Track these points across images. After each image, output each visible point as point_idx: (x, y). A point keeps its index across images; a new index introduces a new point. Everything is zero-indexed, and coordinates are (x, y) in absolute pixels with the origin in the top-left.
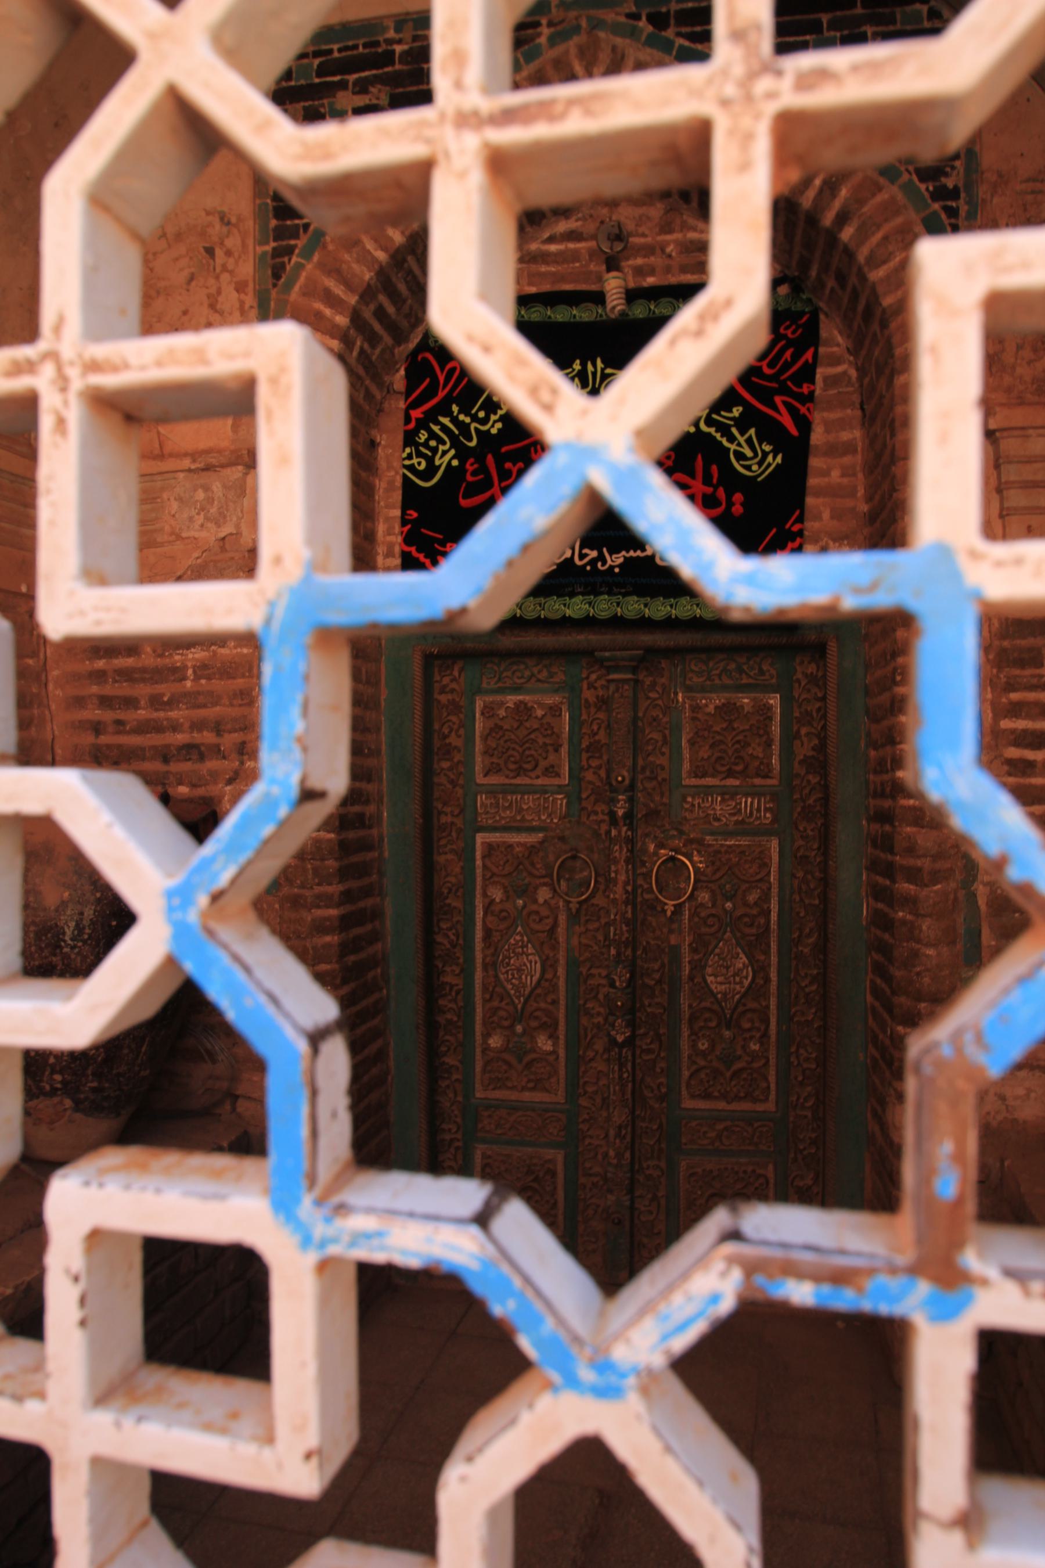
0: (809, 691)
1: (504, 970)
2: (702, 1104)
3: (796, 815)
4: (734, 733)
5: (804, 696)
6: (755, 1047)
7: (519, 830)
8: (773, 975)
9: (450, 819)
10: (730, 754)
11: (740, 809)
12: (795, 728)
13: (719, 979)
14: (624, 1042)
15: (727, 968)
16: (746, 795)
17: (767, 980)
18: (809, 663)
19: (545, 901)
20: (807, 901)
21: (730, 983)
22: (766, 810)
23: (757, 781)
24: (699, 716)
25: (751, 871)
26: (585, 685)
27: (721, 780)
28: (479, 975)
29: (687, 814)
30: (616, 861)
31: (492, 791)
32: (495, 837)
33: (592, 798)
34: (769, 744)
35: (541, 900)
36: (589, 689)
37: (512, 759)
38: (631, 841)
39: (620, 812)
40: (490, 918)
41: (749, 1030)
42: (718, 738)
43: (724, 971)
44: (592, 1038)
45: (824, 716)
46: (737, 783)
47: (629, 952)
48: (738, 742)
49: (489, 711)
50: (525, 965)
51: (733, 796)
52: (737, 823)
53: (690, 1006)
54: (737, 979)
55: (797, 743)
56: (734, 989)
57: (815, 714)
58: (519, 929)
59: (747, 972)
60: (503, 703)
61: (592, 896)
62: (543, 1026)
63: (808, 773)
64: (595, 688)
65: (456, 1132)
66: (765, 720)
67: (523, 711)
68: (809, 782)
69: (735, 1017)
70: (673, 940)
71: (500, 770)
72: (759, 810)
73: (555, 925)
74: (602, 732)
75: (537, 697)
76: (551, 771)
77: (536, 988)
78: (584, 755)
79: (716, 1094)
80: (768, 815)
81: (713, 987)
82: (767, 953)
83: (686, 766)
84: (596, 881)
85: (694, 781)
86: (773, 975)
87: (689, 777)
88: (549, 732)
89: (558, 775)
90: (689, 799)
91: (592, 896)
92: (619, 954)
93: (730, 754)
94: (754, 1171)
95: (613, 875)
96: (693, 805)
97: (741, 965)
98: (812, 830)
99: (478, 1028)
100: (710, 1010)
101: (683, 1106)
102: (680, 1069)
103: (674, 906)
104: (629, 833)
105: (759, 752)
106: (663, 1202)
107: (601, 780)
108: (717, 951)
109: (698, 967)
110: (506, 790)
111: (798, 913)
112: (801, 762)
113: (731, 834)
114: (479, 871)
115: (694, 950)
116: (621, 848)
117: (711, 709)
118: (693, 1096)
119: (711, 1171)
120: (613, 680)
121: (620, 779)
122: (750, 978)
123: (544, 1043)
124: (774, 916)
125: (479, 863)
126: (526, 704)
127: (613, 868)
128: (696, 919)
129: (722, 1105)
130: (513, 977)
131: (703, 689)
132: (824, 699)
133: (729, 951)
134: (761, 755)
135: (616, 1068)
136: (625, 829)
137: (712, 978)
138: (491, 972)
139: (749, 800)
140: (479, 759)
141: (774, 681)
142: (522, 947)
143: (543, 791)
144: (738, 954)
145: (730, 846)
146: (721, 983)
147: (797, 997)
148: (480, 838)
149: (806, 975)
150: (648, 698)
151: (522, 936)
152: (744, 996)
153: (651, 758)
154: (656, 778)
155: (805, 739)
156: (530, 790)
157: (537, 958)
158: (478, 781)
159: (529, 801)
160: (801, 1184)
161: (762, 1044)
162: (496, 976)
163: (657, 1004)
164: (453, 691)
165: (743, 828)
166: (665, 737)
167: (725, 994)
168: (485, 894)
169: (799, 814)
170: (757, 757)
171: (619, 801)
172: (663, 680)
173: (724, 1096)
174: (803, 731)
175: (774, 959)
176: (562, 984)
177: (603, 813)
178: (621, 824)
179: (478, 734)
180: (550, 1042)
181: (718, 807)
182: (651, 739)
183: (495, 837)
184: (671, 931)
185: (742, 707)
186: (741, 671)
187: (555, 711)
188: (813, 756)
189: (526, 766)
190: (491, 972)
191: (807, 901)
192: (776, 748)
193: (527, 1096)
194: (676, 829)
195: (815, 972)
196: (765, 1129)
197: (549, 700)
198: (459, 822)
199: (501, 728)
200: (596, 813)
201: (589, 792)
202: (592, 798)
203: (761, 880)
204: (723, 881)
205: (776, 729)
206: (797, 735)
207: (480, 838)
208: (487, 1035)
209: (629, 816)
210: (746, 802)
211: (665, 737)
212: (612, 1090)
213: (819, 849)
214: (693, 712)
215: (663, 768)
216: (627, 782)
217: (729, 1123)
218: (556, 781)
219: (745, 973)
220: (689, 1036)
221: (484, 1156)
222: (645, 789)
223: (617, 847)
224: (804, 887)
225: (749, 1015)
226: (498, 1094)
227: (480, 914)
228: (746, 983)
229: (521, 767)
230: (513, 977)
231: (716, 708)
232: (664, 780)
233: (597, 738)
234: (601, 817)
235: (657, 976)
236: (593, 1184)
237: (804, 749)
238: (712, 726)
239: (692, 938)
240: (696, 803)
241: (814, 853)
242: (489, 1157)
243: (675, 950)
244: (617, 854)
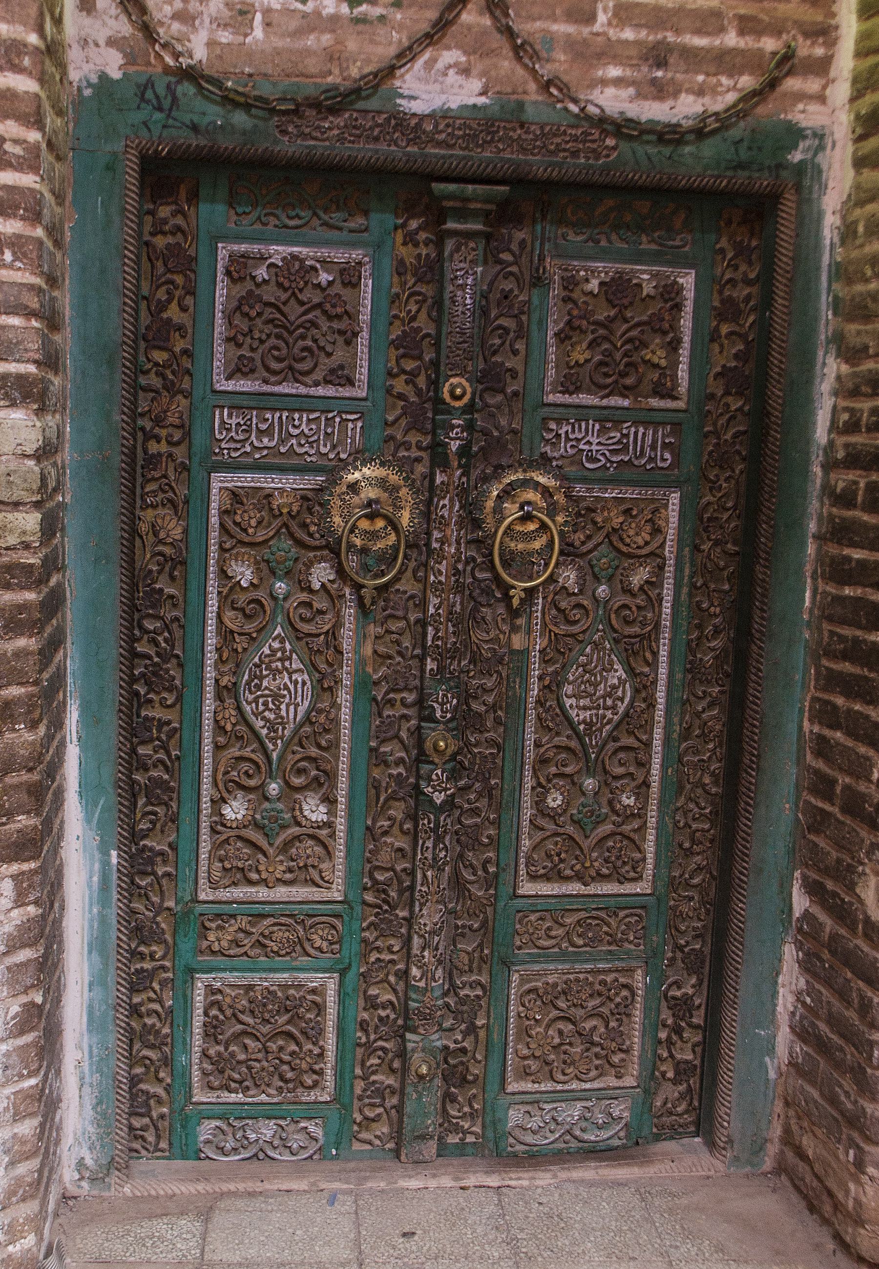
1: (251, 698)
2: (545, 889)
4: (625, 326)
6: (628, 800)
7: (282, 469)
8: (661, 696)
9: (163, 448)
10: (618, 358)
13: (582, 702)
14: (444, 802)
15: (596, 685)
16: (636, 423)
19: (323, 585)
20: (713, 586)
22: (665, 445)
23: (655, 402)
24: (574, 295)
26: (399, 238)
27: (602, 398)
28: (209, 705)
29: (548, 449)
30: (443, 523)
31: (239, 403)
32: (245, 480)
33: (403, 422)
34: (674, 346)
35: (316, 586)
36: (405, 244)
37: (276, 353)
38: (463, 492)
39: (454, 446)
40: (229, 614)
42: (602, 332)
43: (591, 690)
44: (387, 800)
46: (626, 403)
48: (630, 340)
49: (239, 268)
50: (286, 687)
51: (618, 424)
53: (538, 745)
54: (609, 702)
56: (604, 717)
58: (279, 630)
59: (624, 692)
60: (263, 258)
61: (396, 579)
62: (315, 784)
63: (727, 393)
64: (416, 245)
65: (163, 958)
66: (672, 308)
67: (295, 273)
70: (518, 642)
71: (252, 371)
72: (653, 447)
73: (338, 624)
74: (423, 315)
75: (323, 252)
76: (341, 376)
77: (302, 725)
78: (393, 354)
79: (568, 872)
80: (667, 455)
81: (573, 713)
82: (654, 665)
84: (405, 556)
85: (560, 398)
86: (661, 696)
87: (554, 391)
88: (339, 310)
89: (350, 382)
90: (553, 426)
91: (396, 579)
92: (441, 669)
93: (618, 358)
94: (616, 980)
95: (435, 545)
96: (558, 436)
97: (616, 681)
99: (207, 789)
100: (568, 749)
101: (520, 892)
102: (518, 838)
103: (525, 590)
104: (464, 479)
105: (659, 357)
106: (482, 1034)
107: (419, 392)
109: (552, 686)
110: (262, 402)
112: (717, 375)
113: (613, 481)
114: (214, 536)
115: (545, 661)
116: (451, 500)
117: (594, 285)
118: (533, 877)
119: (556, 985)
122: (627, 700)
123: (314, 810)
125: (214, 520)
126: (302, 261)
127: (436, 534)
129: (575, 888)
130: (267, 709)
133: (599, 659)
134: (663, 363)
135: (429, 844)
136: (459, 472)
137: (573, 701)
138: (229, 701)
140: (219, 349)
142: (281, 660)
143: (325, 405)
144: (611, 663)
146: (585, 708)
148: (219, 482)
151: (282, 642)
152: (616, 727)
153: (498, 359)
156: (302, 404)
157: (306, 677)
158: (218, 387)
159: (303, 423)
160: (678, 994)
161: (637, 795)
162: (239, 708)
164: (179, 229)
165: (624, 473)
166: (520, 325)
167: (589, 724)
168: (223, 573)
170: (656, 366)
171: (453, 427)
173: (579, 877)
174: (725, 329)
175: (663, 671)
176: (345, 715)
177: (419, 448)
179: (219, 307)
180: (323, 809)
181: (594, 441)
182: (500, 327)
183: (245, 480)
184: (515, 629)
185: (639, 286)
187: (349, 277)
189: (298, 366)
190: (229, 701)
191: (713, 586)
192: (684, 353)
193: (281, 893)
196: (633, 920)
197: (362, 374)
198: (179, 453)
199: (259, 299)
200: (407, 446)
201: (399, 412)
202: (403, 422)
203: (652, 554)
205: (686, 323)
206: (714, 336)
207: (219, 482)
208: (218, 802)
209: (465, 451)
210: (636, 433)
211: (520, 325)
212: (419, 876)
213: (735, 508)
214: (565, 288)
217: (583, 914)
218: (346, 392)
219: (620, 693)
220: (533, 788)
221: (211, 990)
222: (487, 406)
226: (240, 892)
227: (213, 603)
228: (622, 708)
229: (291, 368)
230: (267, 709)
231: (601, 284)
232: (516, 394)
233: (415, 325)
234: (415, 453)
235: (490, 699)
236: (381, 1019)
237: (724, 357)
238: (593, 313)
239: (546, 642)
240: (562, 432)
241: (725, 516)
242: (220, 991)
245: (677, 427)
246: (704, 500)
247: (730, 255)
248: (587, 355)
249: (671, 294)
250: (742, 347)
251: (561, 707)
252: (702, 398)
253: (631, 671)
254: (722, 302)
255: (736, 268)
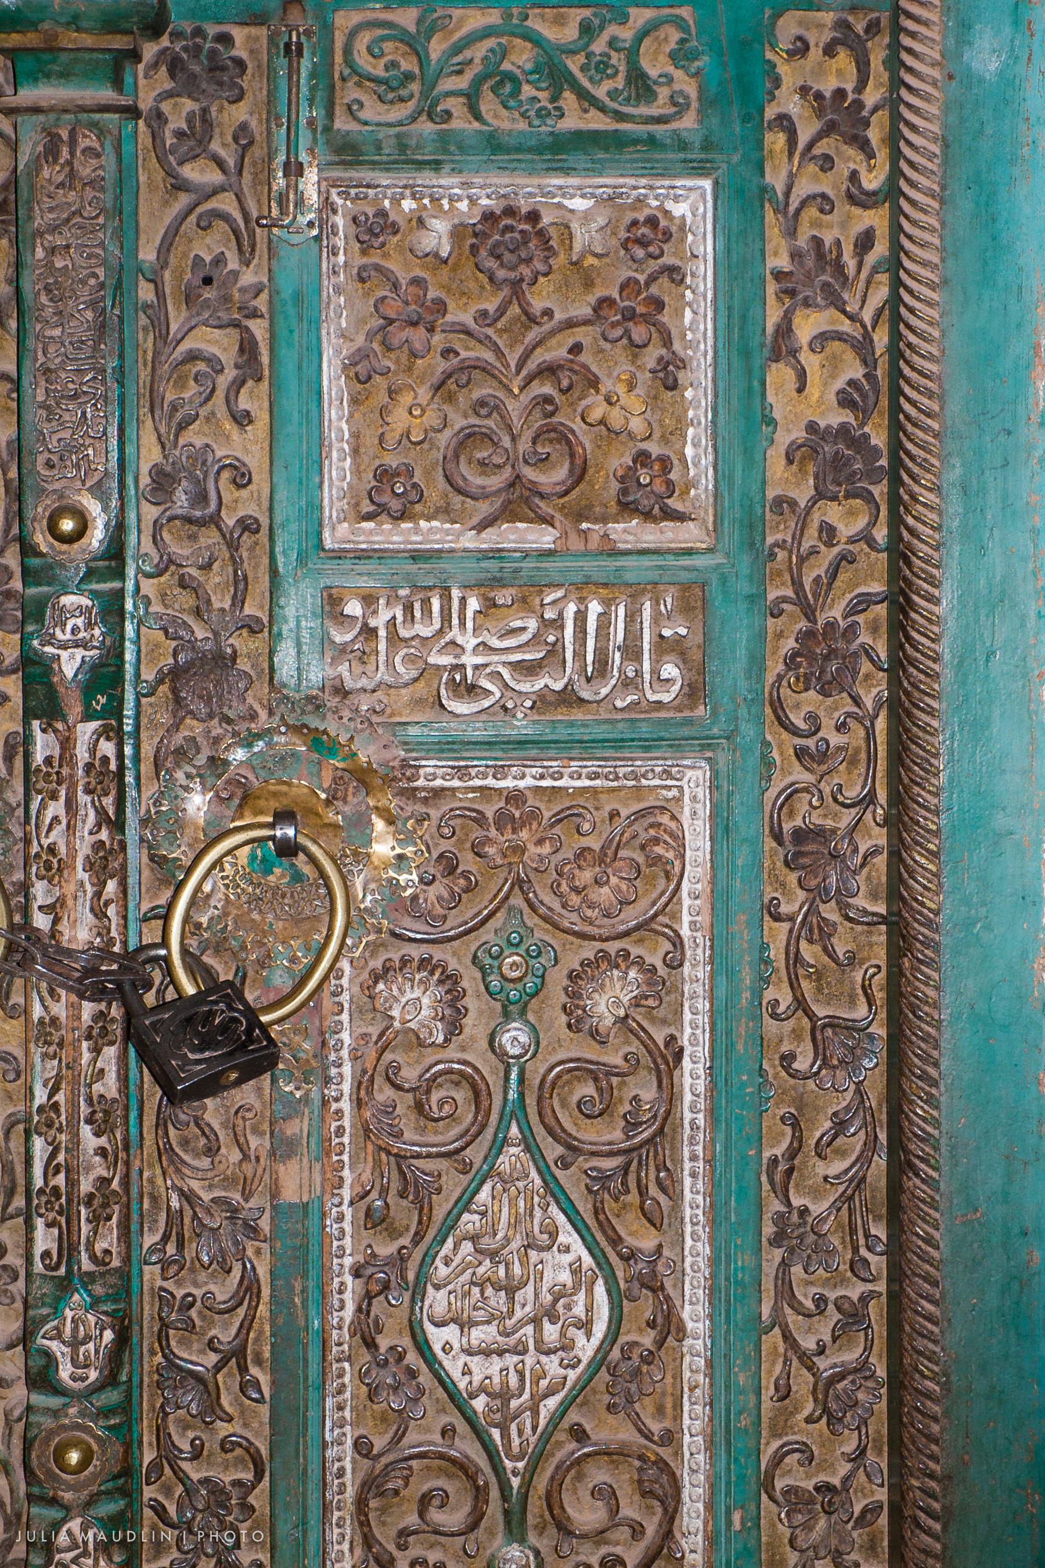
0: (827, 163)
3: (775, 667)
5: (803, 188)
8: (695, 1315)
11: (555, 651)
12: (773, 316)
13: (479, 1335)
15: (511, 1290)
16: (582, 588)
17: (668, 1326)
18: (829, 51)
21: (520, 1350)
23: (627, 532)
25: (604, 895)
30: (54, 867)
39: (70, 664)
41: (599, 1536)
43: (498, 1300)
45: (894, 264)
47: (108, 1240)
48: (550, 371)
52: (543, 701)
53: (362, 1447)
55: (780, 375)
57: (850, 263)
63: (820, 495)
68: (828, 533)
69: (541, 1483)
70: (294, 1181)
72: (631, 651)
80: (670, 670)
81: (453, 1367)
83: (339, 472)
86: (695, 1315)
90: (354, 608)
92: (68, 1247)
96: (370, 632)
98: (841, 728)
108: (470, 1221)
111: (787, 1060)
116: (71, 805)
117: (438, 236)
120: (36, 110)
121: (67, 525)
122: (600, 1329)
124: (693, 1076)
128: (384, 1094)
131: (406, 157)
132: (891, 193)
134: (637, 425)
136: (86, 730)
137: (450, 1333)
139: (595, 608)
141: (688, 122)
144: (553, 1234)
145: (515, 797)
146: (487, 1353)
147: (784, 1393)
149: (821, 1301)
150: (180, 186)
153: (194, 437)
154: (214, 520)
155: (810, 361)
163: (226, 1446)
166: (248, 348)
167: (504, 1395)
169: (791, 661)
172: (240, 113)
174: (807, 326)
175: (696, 1250)
178: (75, 709)
184: (283, 1149)
186: (557, 78)
188: (844, 428)
194: (298, 729)
195: (855, 1291)
204: (487, 934)
205: (696, 322)
206: (782, 345)
210: (581, 617)
211: (248, 348)
215: (242, 478)
216: (97, 537)
223: (56, 808)
224: (809, 952)
225: (599, 1475)
228: (586, 1348)
231: (458, 233)
235: (226, 1333)
240: (379, 621)
241: (848, 817)
243: (300, 1241)
244: (57, 836)
245: (694, 599)
246: (778, 783)
247: (803, 138)
248: (432, 418)
249: (651, 234)
250: (857, 372)
251: (423, 1347)
252: (748, 519)
253: (601, 1235)
254: (795, 255)
255: (827, 163)
